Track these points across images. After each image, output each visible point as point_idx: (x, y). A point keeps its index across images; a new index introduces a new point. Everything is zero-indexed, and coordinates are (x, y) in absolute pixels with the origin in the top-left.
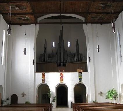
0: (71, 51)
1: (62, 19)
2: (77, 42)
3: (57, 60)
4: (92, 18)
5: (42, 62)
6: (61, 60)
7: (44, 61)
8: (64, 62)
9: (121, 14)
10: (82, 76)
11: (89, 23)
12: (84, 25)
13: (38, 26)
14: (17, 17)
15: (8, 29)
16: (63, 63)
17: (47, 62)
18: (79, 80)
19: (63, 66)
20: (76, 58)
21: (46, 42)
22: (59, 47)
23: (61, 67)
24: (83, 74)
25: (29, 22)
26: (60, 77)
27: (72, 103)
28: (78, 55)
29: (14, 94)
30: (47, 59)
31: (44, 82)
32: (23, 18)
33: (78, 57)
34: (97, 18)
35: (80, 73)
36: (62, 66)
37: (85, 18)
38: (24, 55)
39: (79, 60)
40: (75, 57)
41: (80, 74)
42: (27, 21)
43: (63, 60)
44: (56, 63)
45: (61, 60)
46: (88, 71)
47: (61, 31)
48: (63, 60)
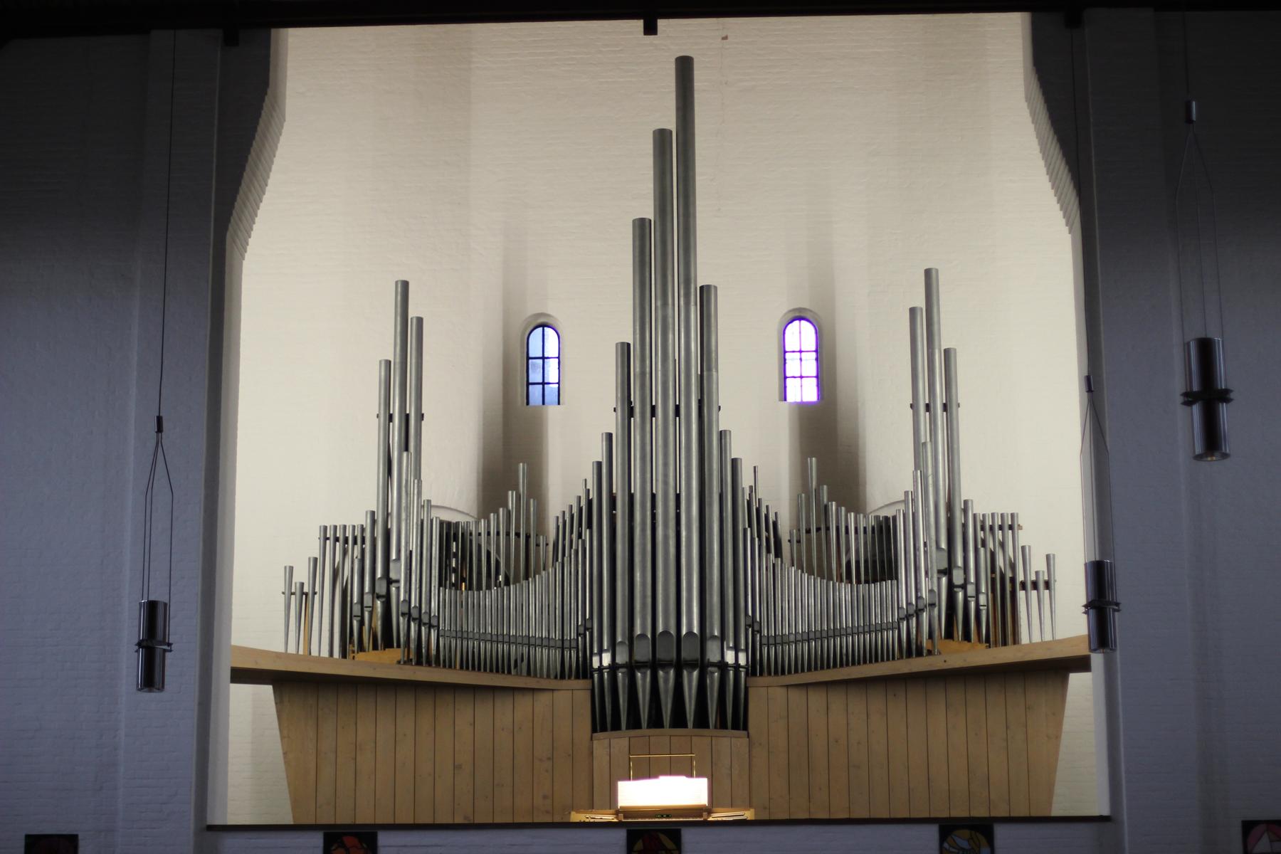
38: (147, 696)
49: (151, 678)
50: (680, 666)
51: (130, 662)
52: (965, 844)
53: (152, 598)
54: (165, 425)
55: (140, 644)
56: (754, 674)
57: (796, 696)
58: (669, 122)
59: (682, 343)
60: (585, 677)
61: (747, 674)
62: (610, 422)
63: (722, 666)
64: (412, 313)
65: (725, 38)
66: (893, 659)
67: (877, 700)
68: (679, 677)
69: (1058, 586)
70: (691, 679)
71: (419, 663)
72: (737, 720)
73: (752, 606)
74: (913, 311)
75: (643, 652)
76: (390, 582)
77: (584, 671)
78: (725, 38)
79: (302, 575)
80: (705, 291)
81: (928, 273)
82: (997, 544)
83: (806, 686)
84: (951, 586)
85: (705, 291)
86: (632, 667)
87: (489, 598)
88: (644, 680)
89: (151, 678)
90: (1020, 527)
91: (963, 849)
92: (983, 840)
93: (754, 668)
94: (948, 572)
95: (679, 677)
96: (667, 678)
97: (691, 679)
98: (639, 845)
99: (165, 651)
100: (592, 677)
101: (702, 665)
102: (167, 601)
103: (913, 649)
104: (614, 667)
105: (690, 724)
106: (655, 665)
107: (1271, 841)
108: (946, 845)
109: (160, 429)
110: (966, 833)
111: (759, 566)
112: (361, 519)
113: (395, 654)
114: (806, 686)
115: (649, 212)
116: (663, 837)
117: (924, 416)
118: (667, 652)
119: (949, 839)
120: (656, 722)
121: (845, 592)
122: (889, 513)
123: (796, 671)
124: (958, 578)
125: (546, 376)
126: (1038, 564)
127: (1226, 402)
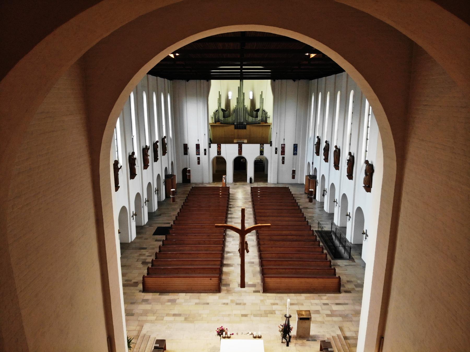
10: (263, 148)
26: (239, 149)
31: (220, 154)
50: (241, 124)
54: (285, 139)
57: (250, 127)
59: (242, 98)
62: (236, 104)
63: (244, 124)
64: (220, 94)
67: (256, 127)
68: (241, 125)
69: (270, 118)
70: (242, 125)
72: (245, 128)
73: (247, 119)
74: (260, 95)
75: (238, 123)
76: (219, 117)
77: (234, 124)
79: (212, 116)
80: (244, 93)
81: (262, 92)
82: (163, 246)
83: (254, 126)
84: (262, 118)
85: (244, 93)
86: (238, 124)
87: (227, 119)
88: (240, 125)
93: (247, 124)
94: (262, 117)
95: (241, 125)
96: (240, 125)
97: (242, 125)
101: (243, 124)
103: (259, 123)
104: (236, 124)
106: (239, 124)
111: (247, 116)
113: (219, 123)
114: (254, 126)
115: (239, 86)
117: (261, 103)
118: (240, 123)
121: (254, 118)
124: (263, 117)
126: (269, 116)
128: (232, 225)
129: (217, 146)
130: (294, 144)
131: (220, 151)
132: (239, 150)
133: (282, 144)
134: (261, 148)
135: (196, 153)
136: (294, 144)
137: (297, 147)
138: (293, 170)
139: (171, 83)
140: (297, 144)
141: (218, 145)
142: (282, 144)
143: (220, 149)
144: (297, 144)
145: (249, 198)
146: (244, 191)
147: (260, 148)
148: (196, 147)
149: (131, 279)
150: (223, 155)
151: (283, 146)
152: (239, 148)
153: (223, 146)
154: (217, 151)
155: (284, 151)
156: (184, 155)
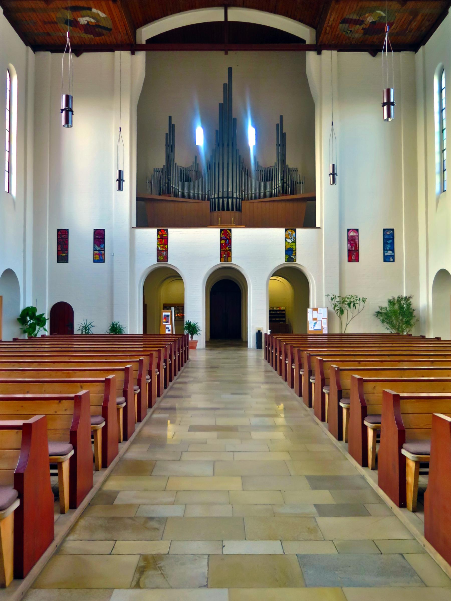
0: (259, 164)
1: (232, 516)
2: (280, 127)
3: (210, 191)
4: (345, 21)
5: (160, 194)
6: (225, 189)
7: (168, 191)
8: (235, 196)
9: (424, 52)
10: (295, 242)
11: (330, 47)
12: (311, 56)
13: (141, 56)
14: (59, 15)
15: (64, 107)
16: (233, 198)
17: (176, 196)
18: (286, 254)
19: (232, 209)
20: (277, 184)
21: (172, 127)
22: (219, 145)
23: (225, 213)
24: (300, 232)
25: (107, 38)
26: (221, 244)
27: (259, 334)
28: (283, 172)
29: (443, 268)
30: (175, 184)
31: (166, 259)
32: (83, 21)
33: (283, 179)
34: (360, 22)
35: (289, 232)
36: (228, 209)
37: (314, 31)
38: (119, 192)
39: (284, 191)
40: (271, 179)
41: (291, 235)
42: (100, 34)
43: (230, 190)
44: (209, 199)
45: (225, 189)
46: (318, 225)
47: (225, 85)
48: (230, 190)
49: (120, 188)
50: (228, 198)
51: (115, 184)
52: (290, 233)
53: (120, 170)
55: (117, 180)
56: (243, 200)
58: (227, 82)
60: (209, 200)
61: (241, 200)
65: (238, 66)
66: (272, 197)
71: (175, 197)
78: (238, 66)
89: (120, 188)
90: (298, 171)
91: (290, 234)
92: (294, 232)
97: (230, 201)
98: (223, 232)
99: (123, 182)
100: (210, 200)
102: (123, 170)
105: (230, 210)
107: (353, 233)
108: (286, 233)
109: (120, 130)
110: (290, 230)
112: (162, 167)
116: (227, 230)
119: (287, 231)
120: (223, 209)
122: (272, 168)
123: (252, 199)
125: (86, 364)
127: (393, 106)
128: (415, 514)
129: (158, 233)
130: (384, 230)
131: (167, 250)
132: (221, 248)
133: (349, 230)
134: (289, 241)
135: (94, 255)
136: (384, 230)
137: (393, 239)
138: (295, 363)
139: (54, 20)
140: (393, 230)
141: (158, 231)
142: (349, 230)
143: (166, 243)
144: (393, 230)
145: (258, 383)
146: (212, 381)
147: (286, 241)
148: (95, 239)
149: (117, 489)
150: (172, 261)
151: (352, 234)
152: (221, 239)
153: (223, 19)
154: (158, 250)
155: (357, 250)
156: (58, 261)
